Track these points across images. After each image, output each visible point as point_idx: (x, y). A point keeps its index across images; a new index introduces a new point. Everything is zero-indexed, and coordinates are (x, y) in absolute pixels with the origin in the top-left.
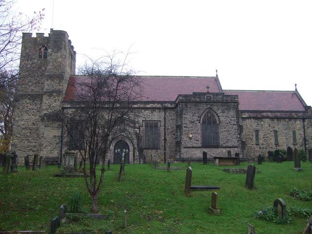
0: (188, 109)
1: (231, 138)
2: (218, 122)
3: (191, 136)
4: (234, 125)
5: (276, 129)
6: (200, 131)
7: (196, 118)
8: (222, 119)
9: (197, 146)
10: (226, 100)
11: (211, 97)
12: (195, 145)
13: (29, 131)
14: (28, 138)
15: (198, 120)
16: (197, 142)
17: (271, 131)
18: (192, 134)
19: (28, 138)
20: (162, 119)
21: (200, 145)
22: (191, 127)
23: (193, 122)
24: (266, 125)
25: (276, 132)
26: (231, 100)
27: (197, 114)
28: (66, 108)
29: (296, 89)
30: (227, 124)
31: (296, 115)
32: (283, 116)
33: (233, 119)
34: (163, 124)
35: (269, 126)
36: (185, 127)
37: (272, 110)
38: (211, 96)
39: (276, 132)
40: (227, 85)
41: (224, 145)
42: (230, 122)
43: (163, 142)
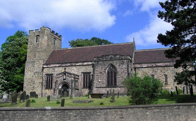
3: (100, 81)
4: (125, 73)
5: (166, 73)
6: (105, 78)
7: (103, 70)
8: (118, 70)
9: (103, 86)
10: (121, 58)
11: (112, 58)
17: (162, 75)
18: (100, 79)
21: (105, 86)
24: (159, 71)
25: (166, 76)
26: (125, 58)
27: (103, 68)
28: (45, 68)
29: (134, 41)
31: (155, 64)
33: (125, 69)
35: (161, 72)
36: (96, 76)
38: (113, 56)
39: (166, 76)
40: (75, 40)
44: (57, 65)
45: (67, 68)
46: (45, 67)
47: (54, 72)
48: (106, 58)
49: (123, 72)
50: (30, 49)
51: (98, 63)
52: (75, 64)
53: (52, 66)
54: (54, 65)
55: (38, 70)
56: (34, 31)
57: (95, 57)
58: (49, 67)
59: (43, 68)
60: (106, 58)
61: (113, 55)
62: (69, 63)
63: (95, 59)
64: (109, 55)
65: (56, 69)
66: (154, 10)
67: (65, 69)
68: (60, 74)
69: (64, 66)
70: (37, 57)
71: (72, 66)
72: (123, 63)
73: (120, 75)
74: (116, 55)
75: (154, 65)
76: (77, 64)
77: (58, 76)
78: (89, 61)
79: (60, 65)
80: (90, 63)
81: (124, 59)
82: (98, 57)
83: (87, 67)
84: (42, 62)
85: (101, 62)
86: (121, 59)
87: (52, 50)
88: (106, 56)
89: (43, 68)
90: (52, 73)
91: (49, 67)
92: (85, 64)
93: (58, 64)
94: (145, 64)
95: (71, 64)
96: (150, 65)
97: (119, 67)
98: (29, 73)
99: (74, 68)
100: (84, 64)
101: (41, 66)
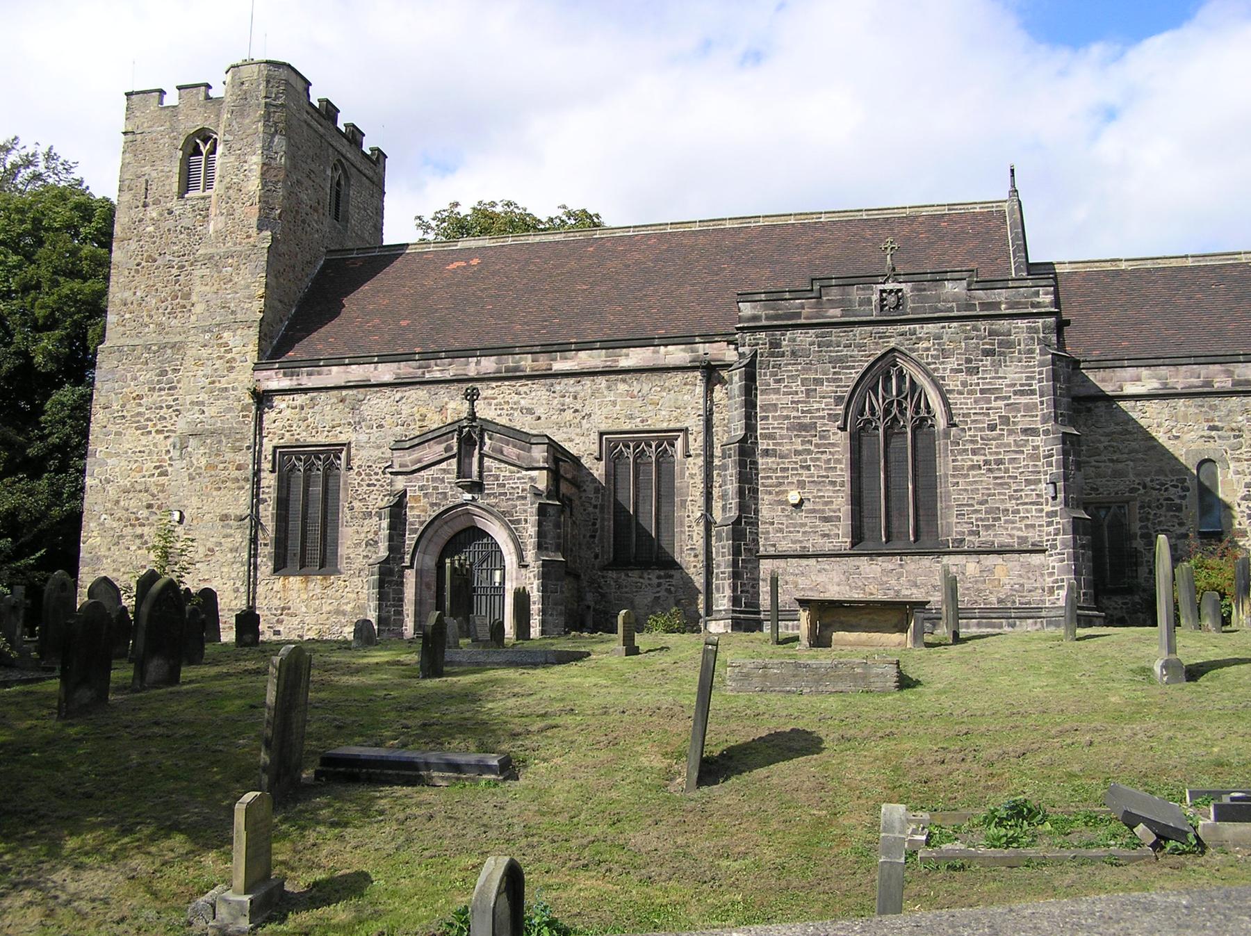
0: (783, 361)
1: (1010, 505)
2: (941, 422)
4: (1025, 431)
9: (827, 546)
10: (984, 305)
12: (816, 543)
13: (146, 498)
14: (139, 530)
15: (833, 418)
16: (826, 527)
18: (801, 485)
19: (139, 530)
20: (695, 424)
22: (797, 453)
23: (803, 427)
27: (827, 387)
30: (992, 428)
31: (1229, 373)
32: (248, 679)
33: (1024, 400)
34: (696, 444)
37: (558, 668)
41: (972, 541)
42: (1005, 420)
43: (699, 530)
44: (386, 372)
45: (485, 391)
46: (273, 385)
47: (355, 426)
48: (844, 304)
49: (1005, 420)
50: (133, 245)
51: (775, 344)
52: (543, 362)
53: (336, 375)
54: (357, 373)
55: (211, 411)
56: (171, 99)
57: (745, 297)
58: (306, 391)
59: (262, 399)
60: (844, 304)
61: (910, 277)
62: (487, 352)
63: (747, 309)
64: (868, 279)
65: (377, 404)
66: (125, 688)
67: (472, 396)
68: (424, 439)
69: (438, 375)
70: (199, 308)
71: (513, 376)
72: (999, 350)
73: (974, 452)
74: (939, 278)
75: (1222, 381)
76: (558, 366)
77: (408, 458)
78: (667, 341)
79: (406, 369)
80: (676, 355)
81: (1004, 309)
82: (774, 296)
83: (644, 385)
84: (245, 344)
85: (804, 338)
86: (978, 312)
87: (317, 258)
88: (847, 282)
89: (262, 399)
90: (343, 438)
91: (306, 391)
92: (634, 357)
93: (384, 359)
94: (1144, 372)
95: (510, 361)
96: (1181, 378)
97: (962, 376)
98: (131, 439)
99: (536, 396)
100: (624, 363)
101: (243, 378)
